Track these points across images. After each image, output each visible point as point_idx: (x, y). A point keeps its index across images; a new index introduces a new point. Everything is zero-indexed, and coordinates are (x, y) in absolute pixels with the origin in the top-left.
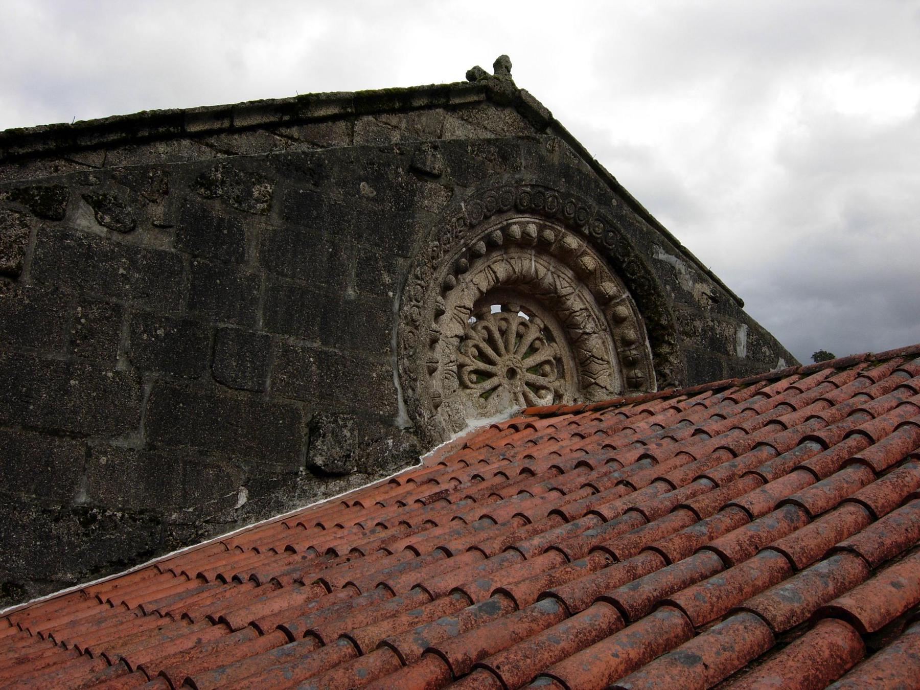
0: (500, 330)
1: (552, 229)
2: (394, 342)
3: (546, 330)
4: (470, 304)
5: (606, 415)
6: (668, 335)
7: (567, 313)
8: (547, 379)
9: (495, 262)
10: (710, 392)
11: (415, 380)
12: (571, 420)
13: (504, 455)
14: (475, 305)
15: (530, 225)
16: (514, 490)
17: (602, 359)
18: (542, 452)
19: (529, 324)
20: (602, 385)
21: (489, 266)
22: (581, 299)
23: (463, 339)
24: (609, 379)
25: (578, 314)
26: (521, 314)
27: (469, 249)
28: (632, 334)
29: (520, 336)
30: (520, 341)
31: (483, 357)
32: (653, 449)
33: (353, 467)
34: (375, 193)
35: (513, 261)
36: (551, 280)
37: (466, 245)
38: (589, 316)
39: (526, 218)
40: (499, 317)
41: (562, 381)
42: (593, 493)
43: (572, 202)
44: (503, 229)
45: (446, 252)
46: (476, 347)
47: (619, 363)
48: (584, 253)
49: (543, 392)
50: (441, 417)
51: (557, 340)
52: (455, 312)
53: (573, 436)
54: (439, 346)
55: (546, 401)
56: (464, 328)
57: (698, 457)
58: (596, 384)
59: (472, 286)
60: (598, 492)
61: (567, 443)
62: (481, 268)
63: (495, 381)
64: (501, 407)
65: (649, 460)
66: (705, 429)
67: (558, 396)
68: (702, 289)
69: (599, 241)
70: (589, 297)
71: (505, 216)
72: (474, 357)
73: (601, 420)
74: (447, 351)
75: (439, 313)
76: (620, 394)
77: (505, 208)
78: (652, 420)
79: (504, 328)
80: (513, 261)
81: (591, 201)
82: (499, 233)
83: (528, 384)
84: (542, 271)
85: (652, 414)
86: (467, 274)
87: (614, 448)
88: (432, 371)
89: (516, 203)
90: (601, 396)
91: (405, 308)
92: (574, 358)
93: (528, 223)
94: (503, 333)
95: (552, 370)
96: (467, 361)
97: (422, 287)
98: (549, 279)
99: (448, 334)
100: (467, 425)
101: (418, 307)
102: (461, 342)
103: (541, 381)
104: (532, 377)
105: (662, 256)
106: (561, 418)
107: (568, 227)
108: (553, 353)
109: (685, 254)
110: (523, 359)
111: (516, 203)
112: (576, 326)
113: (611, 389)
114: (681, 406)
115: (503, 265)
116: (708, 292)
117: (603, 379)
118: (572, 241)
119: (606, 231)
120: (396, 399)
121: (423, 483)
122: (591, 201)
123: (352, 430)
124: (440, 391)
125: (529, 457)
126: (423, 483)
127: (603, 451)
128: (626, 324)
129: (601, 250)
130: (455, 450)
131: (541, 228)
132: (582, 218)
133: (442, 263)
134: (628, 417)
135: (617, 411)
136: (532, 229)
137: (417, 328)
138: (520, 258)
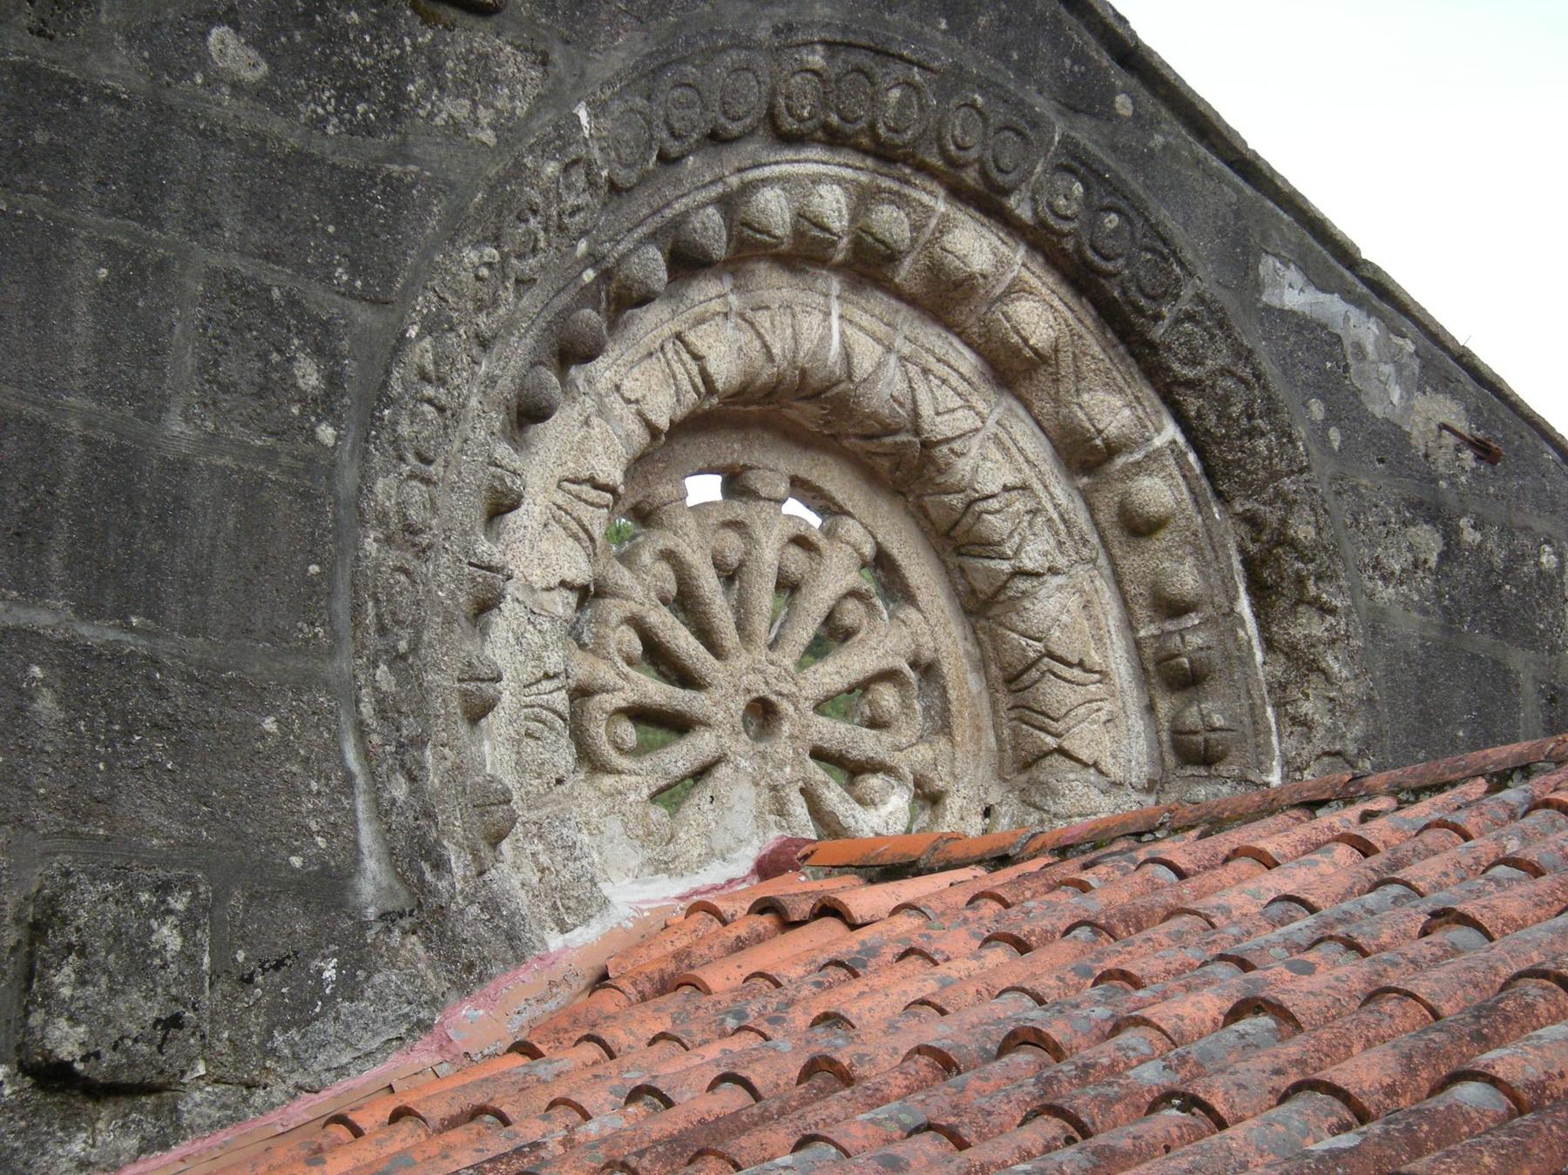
0: (719, 565)
1: (900, 200)
2: (341, 606)
3: (882, 563)
4: (613, 473)
5: (1102, 870)
6: (1319, 578)
7: (956, 500)
8: (886, 737)
9: (700, 321)
10: (1481, 785)
11: (419, 742)
12: (979, 887)
13: (740, 1015)
14: (628, 473)
15: (823, 189)
16: (781, 1136)
17: (1081, 664)
18: (877, 1003)
19: (823, 543)
20: (1084, 755)
21: (679, 336)
22: (1005, 450)
23: (588, 594)
24: (1110, 735)
25: (994, 504)
26: (793, 507)
27: (606, 276)
28: (1186, 579)
29: (788, 586)
30: (791, 605)
31: (657, 656)
32: (1277, 980)
33: (191, 1060)
34: (264, 68)
35: (762, 318)
36: (900, 387)
37: (593, 259)
38: (1034, 512)
39: (811, 162)
40: (715, 518)
41: (942, 744)
42: (1070, 1141)
43: (973, 105)
44: (728, 203)
45: (523, 283)
46: (637, 624)
47: (1143, 675)
48: (1016, 289)
49: (875, 782)
50: (516, 873)
51: (923, 597)
52: (560, 498)
53: (987, 941)
54: (503, 623)
55: (884, 815)
56: (593, 557)
57: (1447, 1008)
58: (1061, 751)
59: (618, 407)
60: (1086, 1133)
61: (968, 963)
62: (651, 340)
63: (702, 744)
64: (728, 840)
65: (1265, 1021)
66: (1469, 908)
67: (929, 797)
68: (1432, 415)
69: (1069, 245)
70: (1034, 445)
71: (734, 157)
72: (630, 662)
73: (1084, 887)
74: (532, 637)
75: (501, 505)
76: (1150, 787)
77: (735, 128)
78: (1275, 882)
79: (733, 558)
80: (762, 318)
81: (1042, 105)
82: (713, 215)
83: (818, 754)
84: (867, 355)
85: (1269, 863)
86: (601, 363)
87: (1136, 983)
88: (478, 711)
89: (772, 107)
90: (1082, 802)
91: (380, 485)
92: (982, 665)
93: (817, 180)
94: (730, 576)
95: (906, 706)
96: (605, 673)
97: (441, 410)
98: (892, 383)
99: (537, 577)
100: (606, 902)
101: (427, 481)
102: (580, 606)
103: (868, 744)
104: (835, 732)
105: (1293, 293)
106: (942, 880)
107: (957, 193)
108: (906, 646)
109: (1380, 293)
110: (801, 665)
111: (772, 107)
112: (988, 547)
113: (1116, 773)
114: (1374, 832)
115: (729, 331)
116: (1462, 426)
117: (1085, 738)
118: (974, 245)
119: (1096, 211)
120: (353, 811)
121: (453, 1123)
122: (1042, 105)
123: (188, 924)
124: (509, 780)
125: (831, 1019)
126: (453, 1123)
127: (1096, 992)
128: (1164, 538)
129: (1079, 276)
130: (563, 994)
131: (863, 199)
132: (1006, 162)
133: (510, 325)
134: (1181, 874)
135: (1142, 855)
136: (832, 204)
137: (422, 552)
138: (788, 306)
